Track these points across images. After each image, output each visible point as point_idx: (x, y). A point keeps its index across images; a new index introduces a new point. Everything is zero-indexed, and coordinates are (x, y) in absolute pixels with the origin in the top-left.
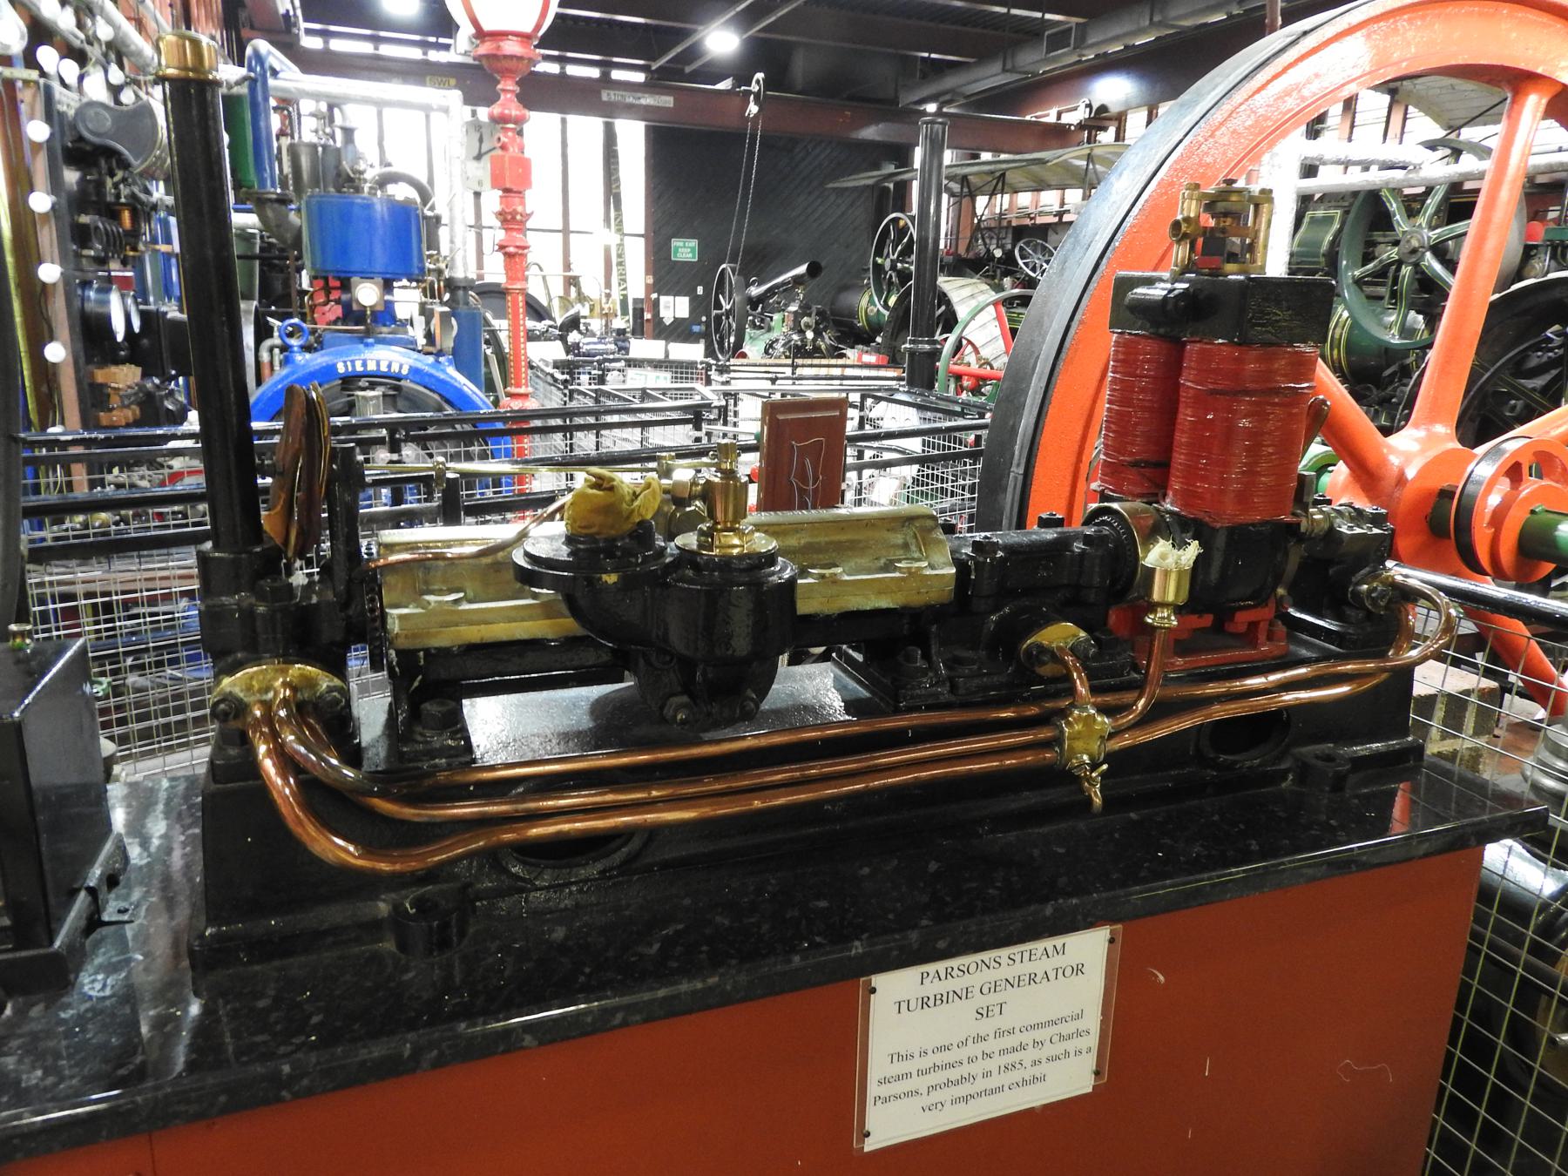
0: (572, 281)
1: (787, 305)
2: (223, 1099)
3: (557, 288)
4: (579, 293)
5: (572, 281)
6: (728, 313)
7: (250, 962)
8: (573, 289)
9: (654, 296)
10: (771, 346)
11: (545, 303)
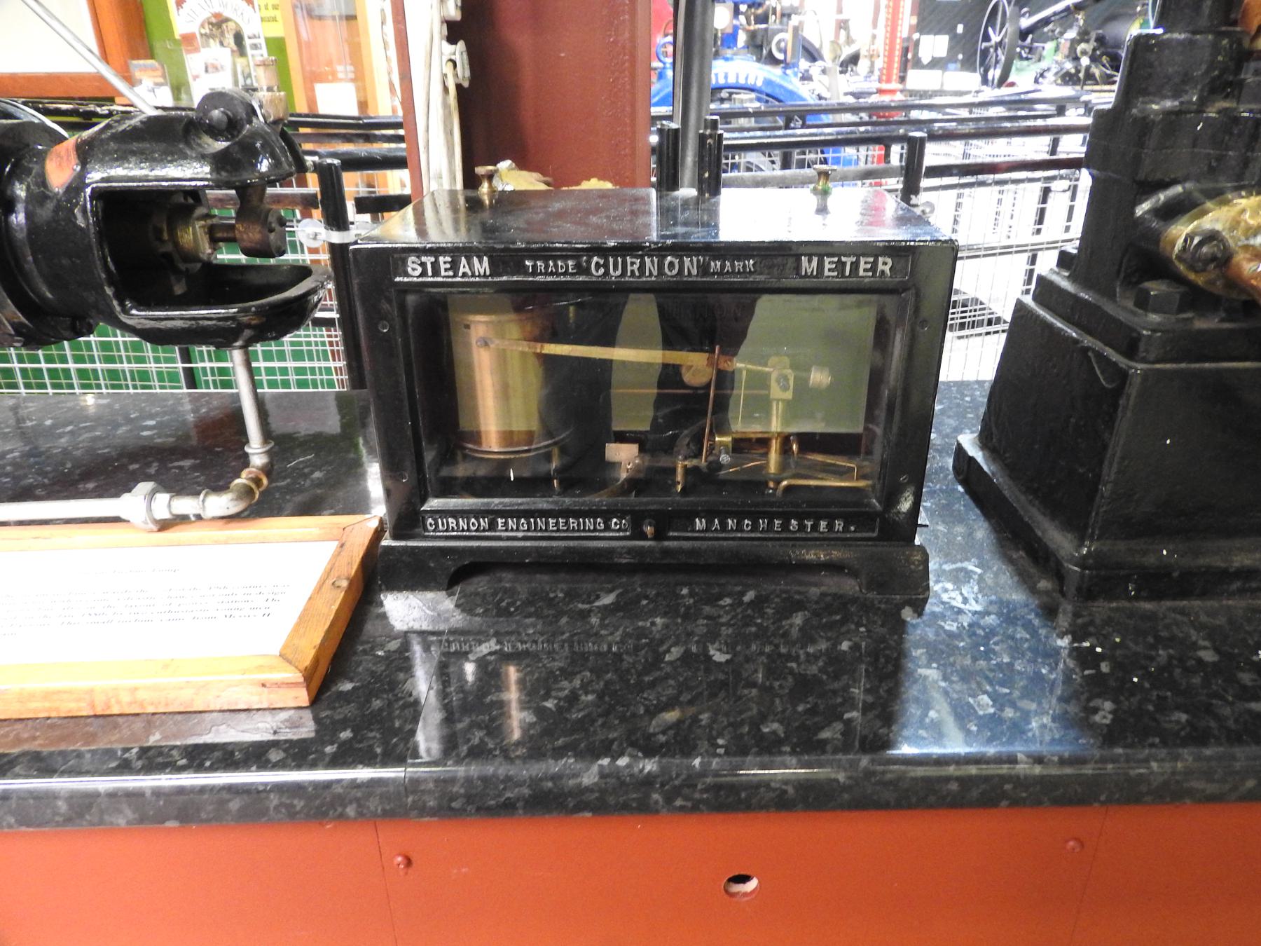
0: (843, 25)
1: (1062, 34)
2: (1250, 783)
3: (829, 35)
4: (848, 37)
5: (843, 25)
6: (1000, 44)
7: (1136, 598)
8: (843, 32)
9: (916, 36)
10: (1042, 75)
11: (817, 46)
